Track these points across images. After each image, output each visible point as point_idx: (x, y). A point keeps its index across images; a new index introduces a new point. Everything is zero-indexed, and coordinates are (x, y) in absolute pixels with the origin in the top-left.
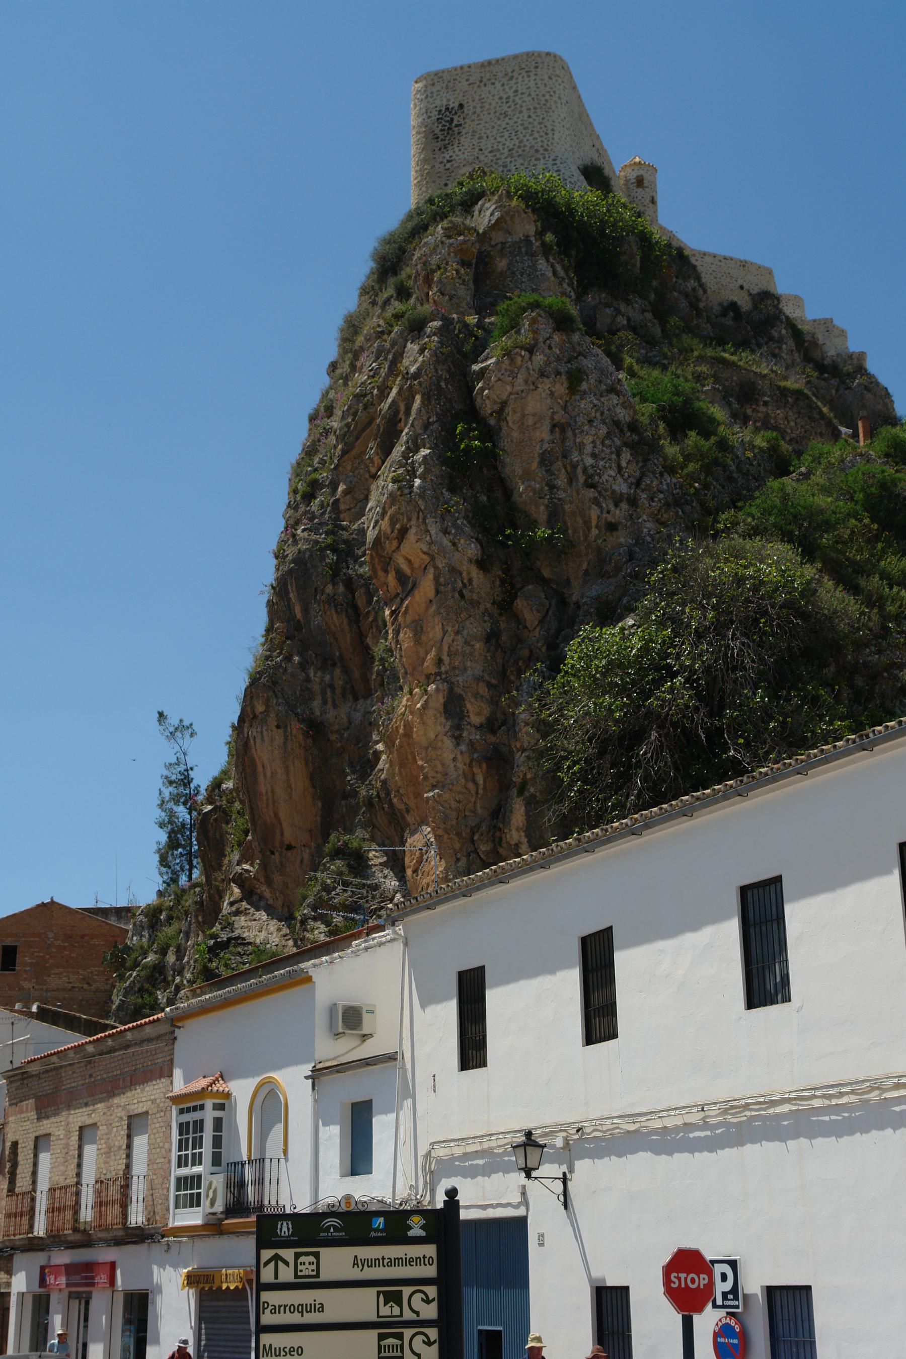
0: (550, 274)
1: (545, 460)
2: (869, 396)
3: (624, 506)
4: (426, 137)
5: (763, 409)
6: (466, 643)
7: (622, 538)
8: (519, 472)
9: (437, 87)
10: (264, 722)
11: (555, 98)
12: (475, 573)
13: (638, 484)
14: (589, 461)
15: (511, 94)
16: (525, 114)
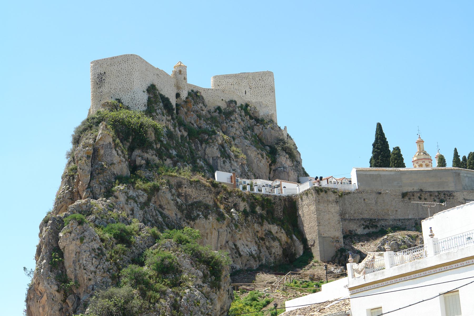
0: (116, 155)
1: (74, 262)
2: (273, 131)
3: (93, 273)
4: (94, 83)
5: (184, 189)
6: (54, 312)
7: (92, 282)
8: (68, 265)
9: (97, 66)
10: (33, 300)
11: (134, 70)
12: (57, 294)
13: (97, 267)
14: (85, 262)
15: (120, 69)
16: (124, 76)
